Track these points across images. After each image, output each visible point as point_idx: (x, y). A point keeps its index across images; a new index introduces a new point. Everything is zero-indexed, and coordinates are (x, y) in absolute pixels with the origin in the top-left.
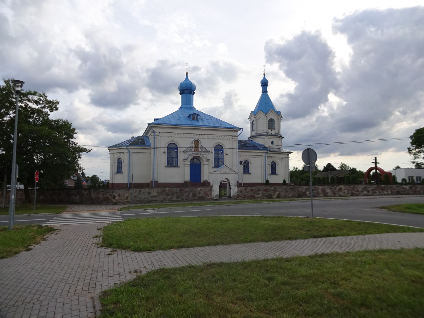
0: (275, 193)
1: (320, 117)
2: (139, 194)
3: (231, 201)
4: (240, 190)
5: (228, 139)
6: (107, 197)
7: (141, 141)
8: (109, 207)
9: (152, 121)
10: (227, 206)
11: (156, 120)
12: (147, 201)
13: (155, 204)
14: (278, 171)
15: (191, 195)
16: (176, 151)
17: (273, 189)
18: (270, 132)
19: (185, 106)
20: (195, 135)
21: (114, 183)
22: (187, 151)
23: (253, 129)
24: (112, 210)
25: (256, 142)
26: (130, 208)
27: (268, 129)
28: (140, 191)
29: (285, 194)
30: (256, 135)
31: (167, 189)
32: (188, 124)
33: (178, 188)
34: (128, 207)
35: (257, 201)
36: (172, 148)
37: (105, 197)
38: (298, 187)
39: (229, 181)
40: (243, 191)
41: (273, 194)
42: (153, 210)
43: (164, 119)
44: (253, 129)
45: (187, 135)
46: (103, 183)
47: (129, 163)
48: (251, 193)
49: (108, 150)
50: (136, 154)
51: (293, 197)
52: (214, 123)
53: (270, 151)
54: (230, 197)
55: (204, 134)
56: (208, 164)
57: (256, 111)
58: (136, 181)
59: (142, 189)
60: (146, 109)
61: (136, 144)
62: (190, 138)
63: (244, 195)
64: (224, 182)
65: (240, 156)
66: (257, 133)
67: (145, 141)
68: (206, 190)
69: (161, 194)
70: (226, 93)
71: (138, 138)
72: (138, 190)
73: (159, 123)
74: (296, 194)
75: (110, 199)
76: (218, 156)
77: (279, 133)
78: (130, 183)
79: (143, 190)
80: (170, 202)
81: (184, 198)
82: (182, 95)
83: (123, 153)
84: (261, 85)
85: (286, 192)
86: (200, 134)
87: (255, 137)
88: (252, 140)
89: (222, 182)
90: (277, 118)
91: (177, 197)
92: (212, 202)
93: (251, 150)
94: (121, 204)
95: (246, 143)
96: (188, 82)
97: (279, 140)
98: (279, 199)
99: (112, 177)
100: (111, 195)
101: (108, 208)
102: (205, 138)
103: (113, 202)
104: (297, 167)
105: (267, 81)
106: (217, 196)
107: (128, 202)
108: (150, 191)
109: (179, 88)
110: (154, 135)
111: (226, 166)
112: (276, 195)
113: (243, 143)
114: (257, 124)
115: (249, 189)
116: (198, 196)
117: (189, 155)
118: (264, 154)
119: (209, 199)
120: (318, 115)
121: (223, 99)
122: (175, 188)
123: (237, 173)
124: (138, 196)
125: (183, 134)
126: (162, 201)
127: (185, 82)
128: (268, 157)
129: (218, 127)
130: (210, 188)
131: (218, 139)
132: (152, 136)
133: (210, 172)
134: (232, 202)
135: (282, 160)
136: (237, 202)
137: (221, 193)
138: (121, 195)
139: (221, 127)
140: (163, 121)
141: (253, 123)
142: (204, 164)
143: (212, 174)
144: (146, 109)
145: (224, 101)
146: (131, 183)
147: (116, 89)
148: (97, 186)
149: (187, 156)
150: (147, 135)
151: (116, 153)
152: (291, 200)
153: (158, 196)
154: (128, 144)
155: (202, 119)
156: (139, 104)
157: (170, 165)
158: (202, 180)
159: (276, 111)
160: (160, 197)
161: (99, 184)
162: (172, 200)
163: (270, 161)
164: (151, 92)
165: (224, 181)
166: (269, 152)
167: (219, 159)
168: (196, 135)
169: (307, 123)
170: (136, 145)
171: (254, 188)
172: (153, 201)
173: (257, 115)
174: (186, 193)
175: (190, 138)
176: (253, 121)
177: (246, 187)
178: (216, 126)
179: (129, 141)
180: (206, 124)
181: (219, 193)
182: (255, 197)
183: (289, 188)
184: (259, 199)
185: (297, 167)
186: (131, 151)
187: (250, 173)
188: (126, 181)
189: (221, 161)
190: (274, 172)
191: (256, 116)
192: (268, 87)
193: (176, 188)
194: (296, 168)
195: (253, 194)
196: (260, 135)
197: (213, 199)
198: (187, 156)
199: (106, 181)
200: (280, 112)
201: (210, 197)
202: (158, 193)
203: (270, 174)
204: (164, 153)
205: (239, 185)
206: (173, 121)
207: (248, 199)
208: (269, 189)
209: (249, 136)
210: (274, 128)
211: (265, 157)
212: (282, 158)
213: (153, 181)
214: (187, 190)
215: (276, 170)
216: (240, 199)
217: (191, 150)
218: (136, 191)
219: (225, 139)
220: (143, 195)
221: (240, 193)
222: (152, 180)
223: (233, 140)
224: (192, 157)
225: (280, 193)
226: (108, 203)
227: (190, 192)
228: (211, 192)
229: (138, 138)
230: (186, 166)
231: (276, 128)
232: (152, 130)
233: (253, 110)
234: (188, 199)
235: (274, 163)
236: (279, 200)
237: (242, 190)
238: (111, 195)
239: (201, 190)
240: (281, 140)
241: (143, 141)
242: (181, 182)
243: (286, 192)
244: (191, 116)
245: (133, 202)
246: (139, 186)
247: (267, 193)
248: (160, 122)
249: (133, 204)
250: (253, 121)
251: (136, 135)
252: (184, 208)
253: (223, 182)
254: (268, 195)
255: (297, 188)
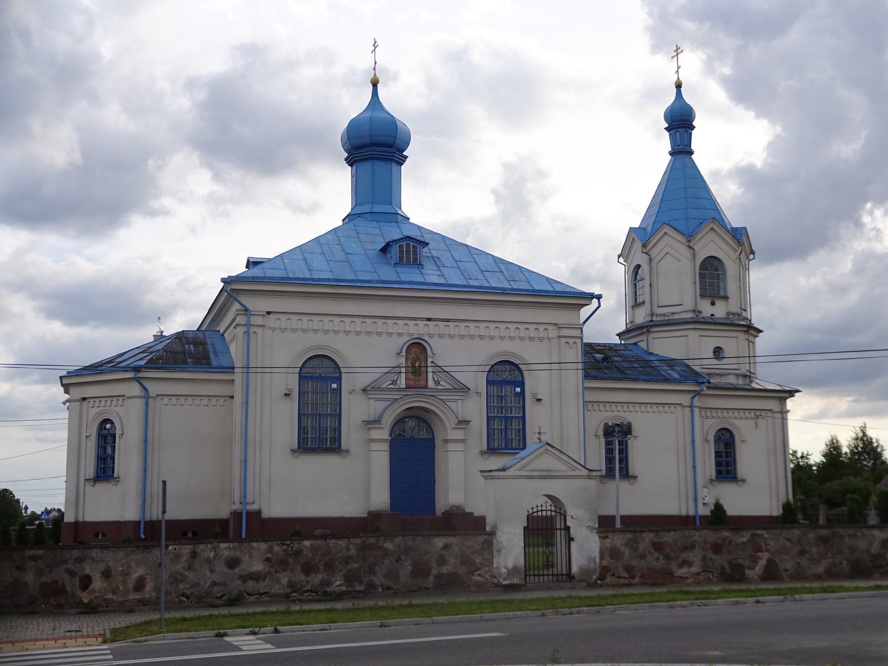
0: (755, 560)
1: (870, 255)
2: (190, 568)
3: (574, 593)
4: (609, 545)
5: (541, 339)
6: (57, 582)
7: (192, 348)
8: (66, 625)
9: (240, 268)
10: (564, 615)
11: (252, 263)
12: (224, 595)
13: (259, 609)
14: (743, 469)
15: (406, 569)
16: (334, 386)
17: (745, 540)
18: (706, 309)
19: (366, 208)
20: (411, 323)
21: (81, 520)
22: (380, 389)
23: (639, 300)
24: (76, 638)
25: (651, 351)
26: (155, 628)
27: (698, 297)
28: (194, 555)
29: (798, 563)
30: (651, 323)
31: (307, 543)
32: (383, 278)
33: (352, 540)
34: (147, 623)
35: (687, 593)
36: (320, 378)
37: (46, 583)
38: (851, 532)
39: (563, 505)
40: (623, 549)
41: (747, 563)
42: (251, 637)
43: (287, 261)
44: (639, 300)
45: (380, 322)
46: (37, 522)
47: (146, 440)
48: (657, 559)
49: (62, 389)
50: (206, 400)
51: (830, 574)
52: (486, 274)
53: (711, 385)
54: (570, 577)
55: (448, 320)
56: (463, 441)
57: (649, 229)
58: (177, 511)
59: (202, 546)
60: (193, 230)
61: (175, 362)
62: (390, 334)
63: (628, 569)
64: (540, 514)
65: (590, 407)
66: (657, 316)
67: (209, 347)
68: (468, 547)
69: (283, 564)
70: (507, 167)
71: (180, 339)
72: (186, 550)
73: (265, 278)
74: (845, 562)
75: (69, 588)
76: (502, 408)
77: (744, 314)
78: (148, 519)
79: (206, 551)
80: (319, 601)
81: (377, 582)
82: (354, 167)
83: (121, 399)
84: (667, 125)
85: (802, 552)
86: (429, 320)
87: (648, 331)
88: (635, 344)
89: (535, 514)
90: (735, 255)
91: (350, 579)
92: (497, 598)
93: (635, 380)
94: (113, 611)
95: (611, 353)
96: (379, 114)
97: (747, 342)
98: (777, 586)
99: (76, 496)
100: (72, 574)
101: (59, 632)
102: (451, 336)
103: (81, 602)
104: (805, 453)
105: (692, 108)
106: (513, 571)
107: (146, 604)
108: (238, 553)
109: (346, 138)
110: (248, 325)
111: (549, 448)
112: (759, 569)
113: (599, 356)
114: (654, 279)
115: (647, 540)
116: (435, 571)
117: (388, 403)
118: (685, 399)
119: (481, 587)
120: (861, 248)
121: (494, 191)
122: (339, 539)
123: (594, 473)
124: (187, 573)
125: (361, 320)
126: (287, 596)
127: (368, 114)
128: (703, 411)
129: (503, 291)
130: (486, 537)
131: (502, 338)
132: (238, 328)
133: (481, 471)
134: (580, 598)
135: (760, 421)
136: (605, 597)
137: (531, 558)
138: (113, 573)
139: (513, 289)
140: (282, 267)
141: (637, 273)
142: (446, 441)
143: (492, 478)
144: (193, 230)
145: (499, 198)
146: (160, 518)
147: (77, 156)
148: (12, 533)
149: (381, 405)
150: (218, 324)
151: (92, 401)
152: (832, 590)
153: (269, 573)
154: (142, 363)
155: (438, 258)
156: (166, 213)
157: (312, 444)
158: (441, 506)
159: (729, 227)
160: (278, 581)
161: (23, 525)
162: (328, 590)
163: (707, 427)
164: (210, 167)
165: (544, 508)
166: (708, 388)
167: (506, 417)
168: (416, 322)
169: (816, 281)
170: (176, 363)
171: (669, 537)
172: (249, 594)
173: (654, 245)
174: (386, 562)
175: (390, 334)
176: (638, 267)
177: (635, 532)
178: (495, 288)
179: (146, 349)
180: (455, 278)
181: (521, 562)
182: (671, 574)
183: (811, 536)
184: (689, 585)
185: (805, 453)
186: (154, 388)
187: (630, 474)
188: (131, 513)
189: (515, 425)
190: (728, 472)
191: (650, 247)
192: (694, 132)
193: (346, 541)
194: (799, 455)
195: (663, 562)
196: (669, 323)
197: (498, 585)
198: (381, 405)
199: (47, 512)
200: (745, 229)
201: (487, 577)
202: (268, 560)
203: (712, 481)
204: (286, 395)
205: (605, 524)
206: (322, 269)
207: (644, 584)
208: (730, 543)
209: (623, 328)
210: (722, 293)
211: (690, 409)
212: (758, 414)
213: (241, 513)
214: (389, 546)
215: (735, 461)
216: (610, 585)
217: (394, 382)
218: (178, 556)
219: (531, 339)
220: (208, 572)
221: (611, 559)
222: (237, 507)
223: (564, 340)
224: (394, 415)
225: (777, 560)
226: (60, 606)
227: (403, 557)
228: (491, 553)
229: (181, 336)
230: (374, 446)
231: (729, 295)
232: (237, 306)
233: (637, 225)
234: (395, 587)
235: (728, 435)
236: (776, 589)
237: (618, 545)
238: (72, 574)
239: (446, 547)
240: (753, 343)
241: (200, 347)
242: (355, 515)
243: (802, 552)
244: (395, 249)
245: (166, 603)
246: (185, 534)
247: (721, 560)
248: (270, 273)
249: (166, 609)
250: (638, 267)
251: (171, 328)
252: (382, 626)
253: (540, 514)
254: (726, 565)
255: (847, 539)
